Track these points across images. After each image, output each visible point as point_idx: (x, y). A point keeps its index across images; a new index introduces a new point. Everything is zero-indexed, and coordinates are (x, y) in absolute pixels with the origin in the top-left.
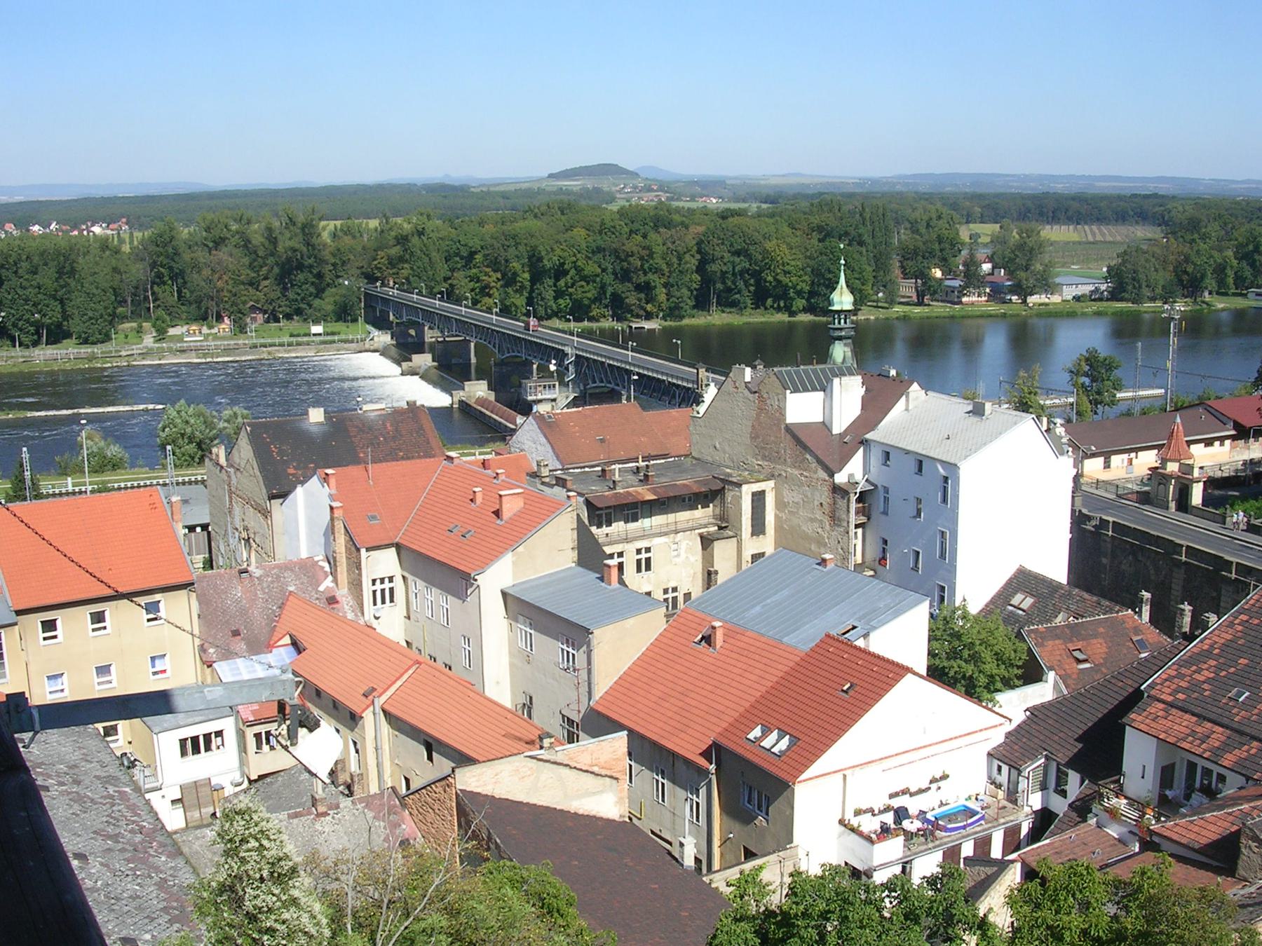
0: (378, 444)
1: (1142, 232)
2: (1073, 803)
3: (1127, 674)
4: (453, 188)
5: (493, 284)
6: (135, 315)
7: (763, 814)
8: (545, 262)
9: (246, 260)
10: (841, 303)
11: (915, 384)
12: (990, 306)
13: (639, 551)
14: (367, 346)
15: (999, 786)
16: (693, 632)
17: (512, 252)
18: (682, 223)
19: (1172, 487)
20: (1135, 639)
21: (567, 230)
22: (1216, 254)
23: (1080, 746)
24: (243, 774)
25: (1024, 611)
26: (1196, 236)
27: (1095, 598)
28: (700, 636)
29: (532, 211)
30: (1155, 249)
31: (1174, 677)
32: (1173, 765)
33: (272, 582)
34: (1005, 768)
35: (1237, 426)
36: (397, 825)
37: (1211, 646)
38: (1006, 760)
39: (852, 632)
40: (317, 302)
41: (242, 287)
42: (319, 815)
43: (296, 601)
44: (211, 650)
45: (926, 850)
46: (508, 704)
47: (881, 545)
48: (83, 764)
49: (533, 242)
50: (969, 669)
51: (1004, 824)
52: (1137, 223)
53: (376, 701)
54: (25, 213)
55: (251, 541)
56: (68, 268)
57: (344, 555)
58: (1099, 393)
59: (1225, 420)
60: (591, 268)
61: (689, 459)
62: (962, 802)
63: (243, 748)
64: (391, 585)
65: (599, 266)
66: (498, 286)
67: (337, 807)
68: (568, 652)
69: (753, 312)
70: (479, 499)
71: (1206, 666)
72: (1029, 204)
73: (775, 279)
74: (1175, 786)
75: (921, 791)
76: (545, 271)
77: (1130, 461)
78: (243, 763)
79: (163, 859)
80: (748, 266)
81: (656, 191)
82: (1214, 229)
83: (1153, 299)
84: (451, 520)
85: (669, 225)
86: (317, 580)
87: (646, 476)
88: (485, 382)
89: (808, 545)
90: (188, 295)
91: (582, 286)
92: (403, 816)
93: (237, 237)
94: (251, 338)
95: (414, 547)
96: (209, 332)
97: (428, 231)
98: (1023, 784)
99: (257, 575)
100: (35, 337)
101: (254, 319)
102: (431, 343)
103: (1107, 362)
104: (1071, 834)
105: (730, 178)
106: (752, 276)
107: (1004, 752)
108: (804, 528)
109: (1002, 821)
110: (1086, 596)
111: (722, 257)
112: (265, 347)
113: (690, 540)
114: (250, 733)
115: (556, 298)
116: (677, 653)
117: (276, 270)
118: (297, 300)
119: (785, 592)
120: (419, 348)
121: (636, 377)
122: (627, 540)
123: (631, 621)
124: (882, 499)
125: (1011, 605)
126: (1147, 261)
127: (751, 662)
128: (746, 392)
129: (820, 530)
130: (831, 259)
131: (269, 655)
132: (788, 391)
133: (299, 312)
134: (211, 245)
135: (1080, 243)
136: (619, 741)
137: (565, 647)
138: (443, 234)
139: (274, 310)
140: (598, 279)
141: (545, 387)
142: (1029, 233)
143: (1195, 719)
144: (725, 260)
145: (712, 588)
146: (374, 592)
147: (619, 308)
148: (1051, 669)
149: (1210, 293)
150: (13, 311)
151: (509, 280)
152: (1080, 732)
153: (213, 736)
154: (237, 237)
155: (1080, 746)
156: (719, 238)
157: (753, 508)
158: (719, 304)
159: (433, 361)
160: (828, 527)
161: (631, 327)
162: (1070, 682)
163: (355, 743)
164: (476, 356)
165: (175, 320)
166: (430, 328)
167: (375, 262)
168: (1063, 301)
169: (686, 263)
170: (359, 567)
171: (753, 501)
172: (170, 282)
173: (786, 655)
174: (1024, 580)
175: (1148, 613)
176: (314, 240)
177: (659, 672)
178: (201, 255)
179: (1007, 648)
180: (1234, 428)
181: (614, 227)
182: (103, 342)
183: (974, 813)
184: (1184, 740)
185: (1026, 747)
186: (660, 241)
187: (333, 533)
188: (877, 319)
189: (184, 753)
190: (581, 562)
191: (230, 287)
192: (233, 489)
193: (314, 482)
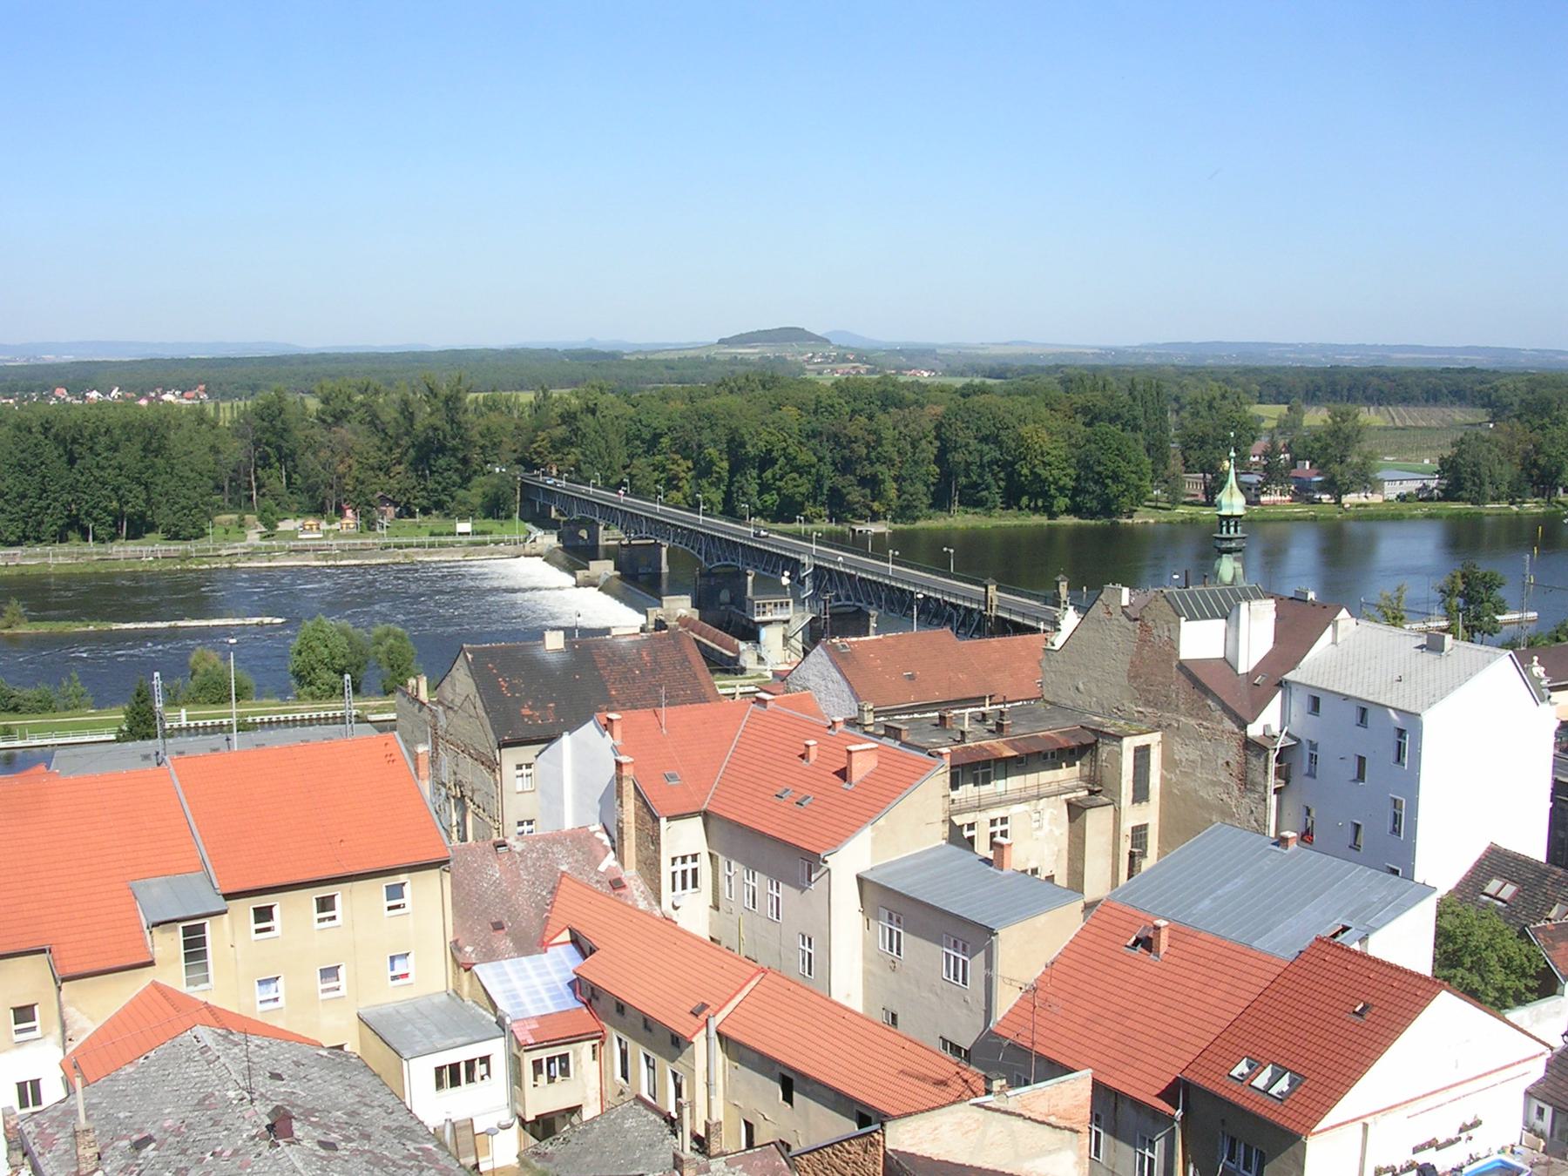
0: (633, 679)
1: (1461, 415)
5: (683, 474)
6: (236, 505)
8: (749, 448)
10: (1231, 506)
11: (1344, 610)
12: (1296, 507)
13: (993, 822)
14: (528, 549)
15: (1540, 1135)
17: (707, 435)
21: (774, 409)
25: (1504, 901)
26: (1546, 420)
28: (1134, 938)
33: (539, 859)
40: (461, 493)
41: (371, 473)
44: (469, 949)
48: (363, 1109)
49: (734, 423)
52: (1452, 403)
53: (711, 1021)
54: (37, 379)
56: (155, 445)
57: (633, 825)
58: (1477, 618)
60: (805, 457)
62: (1497, 1157)
63: (516, 1078)
64: (695, 865)
65: (815, 454)
66: (689, 477)
69: (1004, 512)
73: (1032, 472)
75: (1450, 1143)
80: (998, 456)
81: (852, 361)
83: (1494, 500)
84: (778, 782)
85: (900, 404)
86: (595, 858)
87: (1000, 727)
88: (688, 597)
89: (1207, 816)
90: (299, 481)
91: (794, 479)
94: (380, 537)
95: (732, 817)
96: (328, 527)
99: (518, 849)
100: (113, 530)
102: (607, 547)
105: (941, 347)
106: (1003, 467)
107: (1547, 1090)
111: (967, 444)
112: (400, 547)
113: (1055, 808)
114: (527, 1060)
115: (760, 493)
118: (436, 490)
122: (979, 808)
124: (1307, 757)
125: (1486, 894)
126: (1490, 451)
127: (1212, 974)
128: (1123, 619)
129: (1225, 797)
130: (1101, 448)
131: (544, 956)
132: (1183, 619)
133: (439, 505)
134: (330, 420)
135: (1386, 429)
138: (619, 411)
139: (408, 502)
140: (813, 471)
141: (776, 605)
144: (971, 449)
145: (1136, 877)
146: (674, 873)
147: (838, 507)
150: (86, 497)
151: (703, 470)
153: (477, 1062)
154: (363, 410)
157: (1135, 767)
158: (961, 503)
159: (615, 569)
160: (1236, 793)
161: (854, 530)
163: (675, 1075)
164: (668, 562)
165: (286, 511)
166: (605, 529)
167: (535, 445)
168: (1385, 501)
170: (656, 840)
171: (1135, 757)
172: (277, 464)
174: (1496, 862)
176: (460, 417)
178: (319, 434)
179: (1513, 947)
181: (832, 406)
182: (197, 538)
186: (890, 423)
188: (1157, 523)
189: (439, 1084)
192: (440, 733)
193: (589, 730)
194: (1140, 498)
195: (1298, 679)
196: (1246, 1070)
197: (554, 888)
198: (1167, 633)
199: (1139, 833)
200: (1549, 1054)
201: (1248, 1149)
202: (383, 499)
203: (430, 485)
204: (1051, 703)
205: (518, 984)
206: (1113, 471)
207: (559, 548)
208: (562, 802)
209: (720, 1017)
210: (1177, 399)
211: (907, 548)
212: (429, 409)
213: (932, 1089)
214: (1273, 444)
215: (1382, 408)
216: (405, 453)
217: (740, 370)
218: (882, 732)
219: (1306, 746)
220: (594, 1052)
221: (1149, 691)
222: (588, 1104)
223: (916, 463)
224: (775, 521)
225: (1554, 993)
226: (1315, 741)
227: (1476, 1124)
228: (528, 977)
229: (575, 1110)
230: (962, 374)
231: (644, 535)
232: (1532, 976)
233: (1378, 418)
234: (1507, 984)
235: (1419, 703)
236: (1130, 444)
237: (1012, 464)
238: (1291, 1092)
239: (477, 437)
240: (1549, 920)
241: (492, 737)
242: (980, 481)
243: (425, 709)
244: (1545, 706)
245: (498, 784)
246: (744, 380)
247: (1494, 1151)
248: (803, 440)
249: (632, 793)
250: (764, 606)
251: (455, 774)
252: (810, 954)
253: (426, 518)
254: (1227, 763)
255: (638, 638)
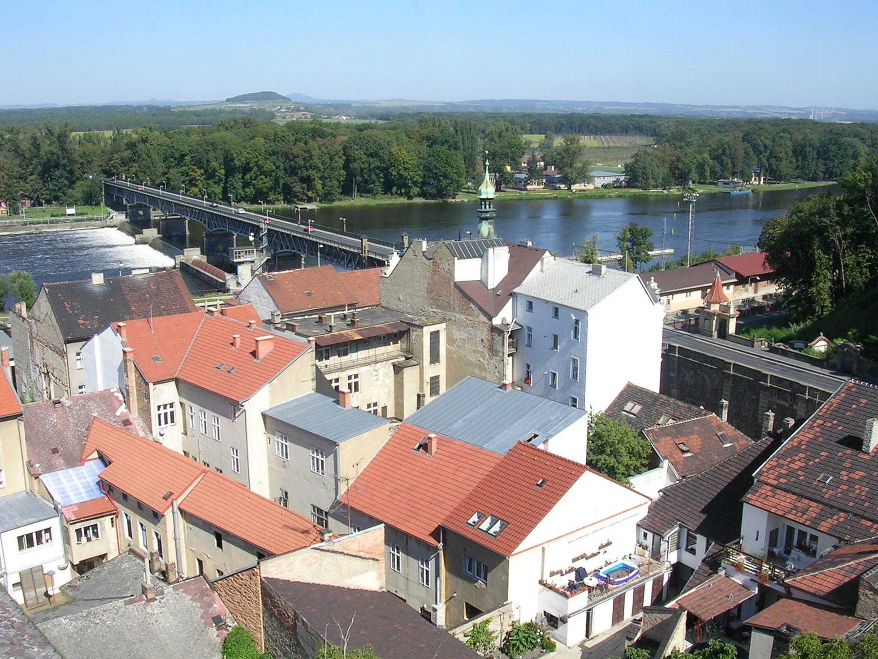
1: (640, 141)
2: (705, 559)
3: (731, 463)
4: (158, 108)
5: (198, 178)
7: (482, 579)
8: (236, 161)
9: (17, 161)
10: (487, 193)
12: (546, 192)
13: (350, 378)
14: (108, 223)
15: (645, 548)
16: (412, 441)
18: (331, 134)
19: (714, 321)
20: (719, 434)
21: (250, 139)
22: (698, 156)
23: (704, 516)
24: (67, 560)
25: (634, 415)
27: (687, 405)
28: (418, 444)
29: (224, 125)
30: (657, 152)
31: (776, 466)
32: (777, 530)
33: (80, 410)
34: (650, 535)
35: (738, 275)
36: (210, 605)
37: (799, 443)
38: (652, 529)
39: (534, 440)
40: (70, 191)
42: (149, 601)
43: (98, 424)
44: (37, 465)
45: (603, 599)
46: (267, 496)
47: (525, 369)
49: (227, 147)
50: (612, 461)
51: (653, 576)
52: (636, 134)
53: (174, 502)
55: (50, 375)
57: (135, 388)
58: (638, 253)
59: (729, 271)
60: (269, 166)
61: (379, 308)
62: (621, 561)
63: (67, 540)
64: (172, 410)
65: (274, 165)
66: (202, 179)
67: (162, 593)
68: (282, 444)
69: (383, 196)
70: (238, 343)
71: (797, 458)
72: (563, 121)
73: (398, 173)
74: (778, 544)
75: (594, 555)
76: (236, 168)
77: (668, 301)
78: (68, 551)
79: (36, 649)
82: (695, 139)
83: (656, 187)
84: (218, 360)
85: (322, 135)
86: (114, 408)
87: (353, 322)
88: (199, 249)
89: (472, 370)
92: (213, 597)
93: (9, 144)
94: (22, 218)
97: (150, 139)
98: (664, 546)
99: (68, 405)
101: (23, 204)
102: (155, 221)
103: (643, 232)
104: (709, 583)
105: (355, 102)
106: (382, 171)
107: (649, 523)
108: (469, 357)
109: (651, 574)
110: (680, 403)
112: (33, 223)
113: (386, 368)
114: (72, 529)
115: (243, 188)
116: (401, 457)
117: (39, 168)
118: (55, 190)
119: (478, 410)
120: (146, 223)
121: (322, 246)
122: (341, 369)
123: (366, 435)
124: (527, 337)
128: (424, 259)
129: (481, 359)
130: (437, 160)
131: (82, 467)
133: (56, 198)
135: (598, 148)
136: (378, 532)
137: (315, 455)
138: (161, 141)
139: (38, 197)
140: (273, 174)
142: (572, 141)
143: (795, 497)
146: (159, 415)
147: (289, 195)
148: (665, 458)
149: (694, 182)
151: (210, 175)
152: (703, 507)
153: (43, 532)
154: (9, 144)
155: (704, 516)
156: (357, 145)
158: (358, 191)
159: (159, 233)
160: (487, 357)
162: (679, 467)
163: (157, 534)
166: (154, 210)
167: (112, 162)
169: (336, 162)
170: (147, 396)
171: (431, 338)
173: (487, 458)
174: (631, 393)
175: (726, 415)
177: (389, 473)
180: (736, 277)
181: (284, 137)
183: (632, 570)
184: (789, 512)
185: (663, 518)
187: (126, 371)
188: (469, 201)
189: (21, 547)
190: (319, 389)
191: (6, 181)
192: (34, 335)
193: (109, 332)
194: (459, 188)
195: (521, 292)
196: (476, 520)
197: (89, 426)
198: (447, 267)
199: (435, 381)
200: (649, 503)
201: (479, 565)
202: (23, 196)
203: (51, 187)
204: (385, 308)
205: (66, 485)
206: (444, 173)
207: (127, 222)
208: (95, 375)
209: (180, 500)
210: (483, 132)
211: (326, 219)
212: (48, 142)
213: (302, 535)
214: (534, 157)
215: (597, 136)
216: (34, 169)
217: (238, 116)
218: (285, 327)
219: (526, 330)
220: (112, 522)
221: (439, 300)
222: (111, 553)
223: (332, 169)
224: (252, 203)
225: (658, 467)
226: (530, 326)
227: (609, 544)
228: (72, 480)
229: (104, 556)
230: (365, 118)
231: (174, 213)
232: (644, 458)
233: (595, 142)
234: (630, 462)
235: (586, 304)
236: (453, 157)
237: (387, 169)
238: (500, 532)
239: (78, 158)
240: (659, 425)
241: (61, 337)
242: (369, 179)
243: (25, 321)
244: (657, 305)
245: (67, 364)
246: (233, 123)
247: (620, 558)
248: (268, 157)
249: (133, 369)
250: (239, 253)
251: (43, 359)
252: (237, 459)
253: (49, 206)
254: (482, 340)
255: (148, 276)
